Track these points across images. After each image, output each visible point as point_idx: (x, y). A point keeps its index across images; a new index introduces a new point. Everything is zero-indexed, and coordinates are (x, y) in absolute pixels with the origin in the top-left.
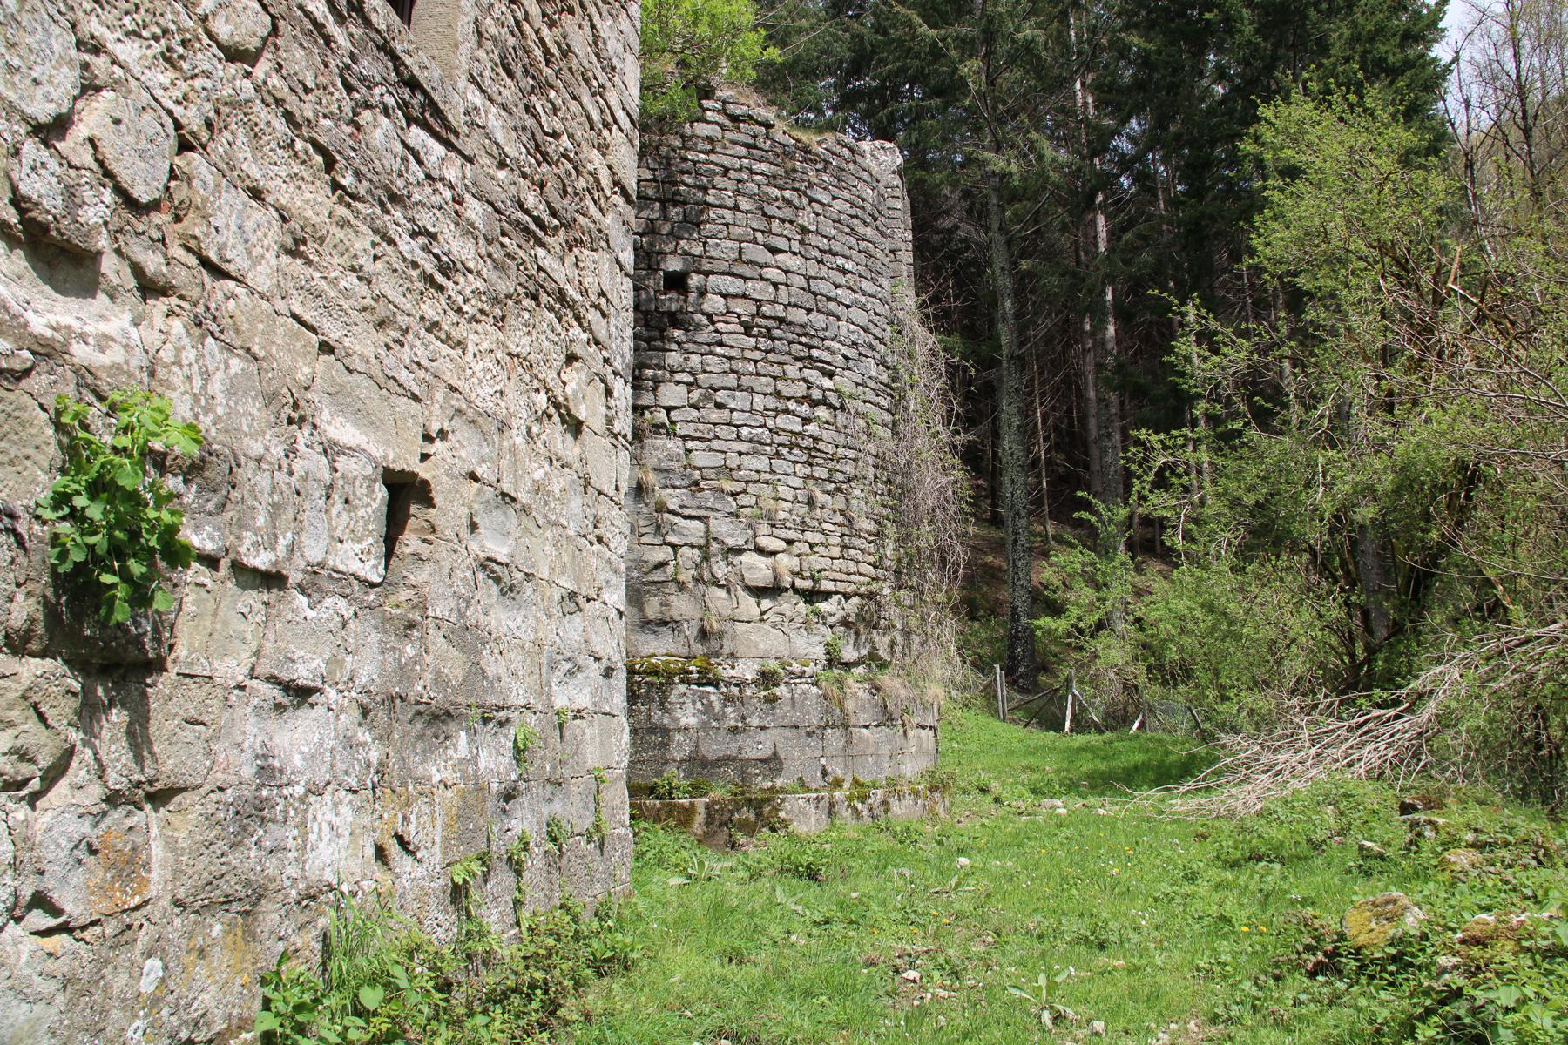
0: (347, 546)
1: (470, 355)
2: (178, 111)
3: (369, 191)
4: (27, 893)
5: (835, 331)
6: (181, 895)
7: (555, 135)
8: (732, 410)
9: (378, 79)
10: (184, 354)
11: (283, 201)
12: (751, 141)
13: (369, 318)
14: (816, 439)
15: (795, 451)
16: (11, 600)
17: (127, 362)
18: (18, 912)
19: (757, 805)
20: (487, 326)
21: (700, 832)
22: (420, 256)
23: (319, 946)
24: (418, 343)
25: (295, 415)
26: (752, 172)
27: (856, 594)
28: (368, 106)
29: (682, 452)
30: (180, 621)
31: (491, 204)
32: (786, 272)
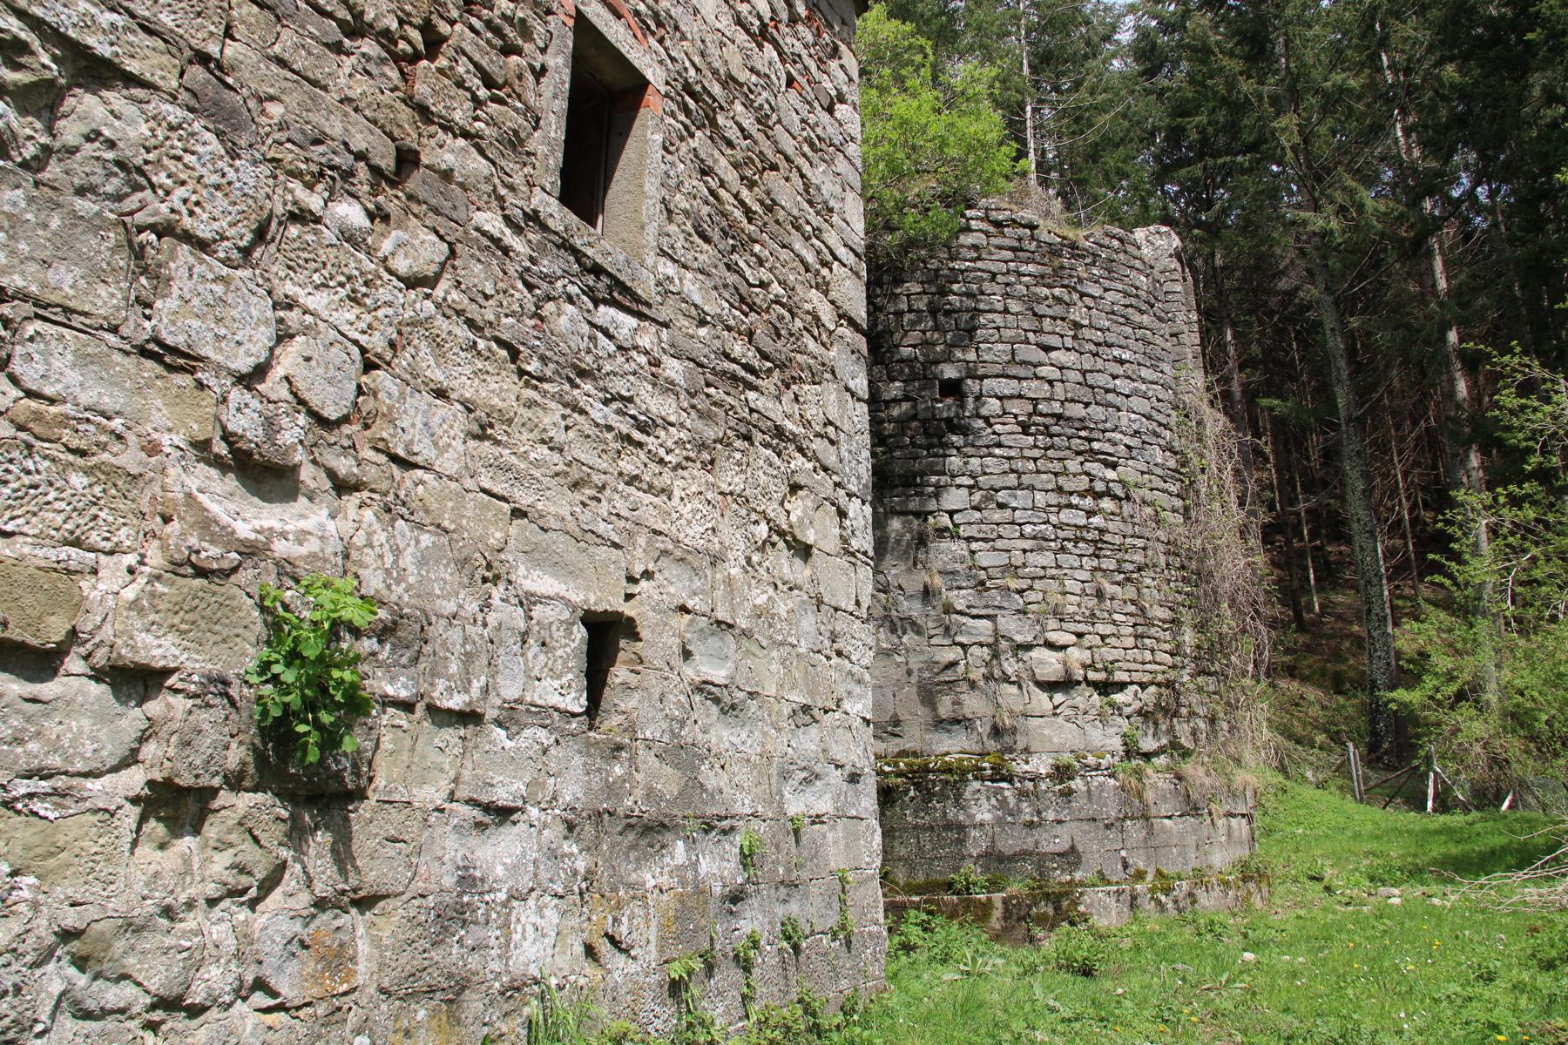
0: (546, 683)
1: (676, 500)
2: (363, 339)
3: (556, 372)
4: (249, 978)
5: (1116, 422)
6: (386, 984)
7: (762, 285)
8: (1014, 509)
9: (560, 272)
10: (375, 537)
11: (468, 395)
12: (1016, 244)
13: (563, 481)
14: (1102, 531)
15: (1081, 545)
16: (227, 748)
17: (322, 550)
18: (243, 993)
19: (1055, 899)
20: (695, 471)
21: (998, 926)
22: (614, 420)
23: (524, 1032)
24: (617, 497)
25: (489, 575)
27: (1152, 683)
28: (549, 298)
30: (378, 757)
31: (693, 360)
32: (1061, 369)
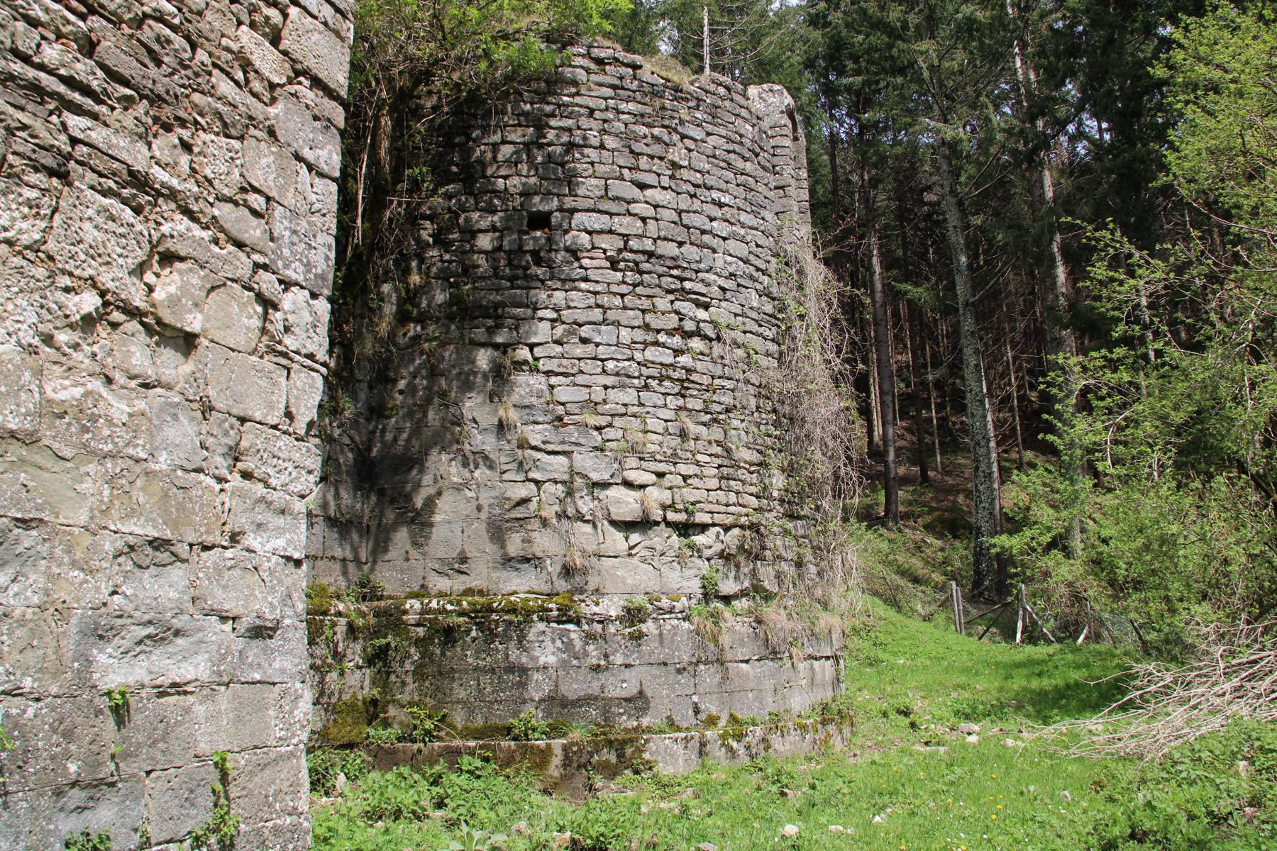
5: (710, 263)
8: (597, 345)
12: (617, 82)
14: (689, 371)
19: (619, 746)
21: (556, 774)
26: (619, 112)
29: (545, 388)
32: (656, 207)
